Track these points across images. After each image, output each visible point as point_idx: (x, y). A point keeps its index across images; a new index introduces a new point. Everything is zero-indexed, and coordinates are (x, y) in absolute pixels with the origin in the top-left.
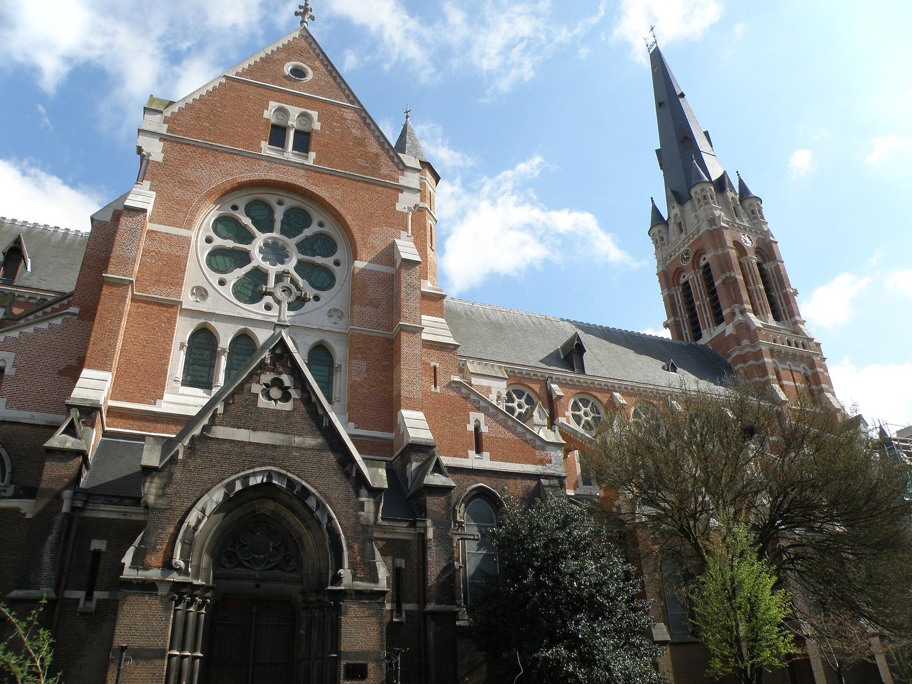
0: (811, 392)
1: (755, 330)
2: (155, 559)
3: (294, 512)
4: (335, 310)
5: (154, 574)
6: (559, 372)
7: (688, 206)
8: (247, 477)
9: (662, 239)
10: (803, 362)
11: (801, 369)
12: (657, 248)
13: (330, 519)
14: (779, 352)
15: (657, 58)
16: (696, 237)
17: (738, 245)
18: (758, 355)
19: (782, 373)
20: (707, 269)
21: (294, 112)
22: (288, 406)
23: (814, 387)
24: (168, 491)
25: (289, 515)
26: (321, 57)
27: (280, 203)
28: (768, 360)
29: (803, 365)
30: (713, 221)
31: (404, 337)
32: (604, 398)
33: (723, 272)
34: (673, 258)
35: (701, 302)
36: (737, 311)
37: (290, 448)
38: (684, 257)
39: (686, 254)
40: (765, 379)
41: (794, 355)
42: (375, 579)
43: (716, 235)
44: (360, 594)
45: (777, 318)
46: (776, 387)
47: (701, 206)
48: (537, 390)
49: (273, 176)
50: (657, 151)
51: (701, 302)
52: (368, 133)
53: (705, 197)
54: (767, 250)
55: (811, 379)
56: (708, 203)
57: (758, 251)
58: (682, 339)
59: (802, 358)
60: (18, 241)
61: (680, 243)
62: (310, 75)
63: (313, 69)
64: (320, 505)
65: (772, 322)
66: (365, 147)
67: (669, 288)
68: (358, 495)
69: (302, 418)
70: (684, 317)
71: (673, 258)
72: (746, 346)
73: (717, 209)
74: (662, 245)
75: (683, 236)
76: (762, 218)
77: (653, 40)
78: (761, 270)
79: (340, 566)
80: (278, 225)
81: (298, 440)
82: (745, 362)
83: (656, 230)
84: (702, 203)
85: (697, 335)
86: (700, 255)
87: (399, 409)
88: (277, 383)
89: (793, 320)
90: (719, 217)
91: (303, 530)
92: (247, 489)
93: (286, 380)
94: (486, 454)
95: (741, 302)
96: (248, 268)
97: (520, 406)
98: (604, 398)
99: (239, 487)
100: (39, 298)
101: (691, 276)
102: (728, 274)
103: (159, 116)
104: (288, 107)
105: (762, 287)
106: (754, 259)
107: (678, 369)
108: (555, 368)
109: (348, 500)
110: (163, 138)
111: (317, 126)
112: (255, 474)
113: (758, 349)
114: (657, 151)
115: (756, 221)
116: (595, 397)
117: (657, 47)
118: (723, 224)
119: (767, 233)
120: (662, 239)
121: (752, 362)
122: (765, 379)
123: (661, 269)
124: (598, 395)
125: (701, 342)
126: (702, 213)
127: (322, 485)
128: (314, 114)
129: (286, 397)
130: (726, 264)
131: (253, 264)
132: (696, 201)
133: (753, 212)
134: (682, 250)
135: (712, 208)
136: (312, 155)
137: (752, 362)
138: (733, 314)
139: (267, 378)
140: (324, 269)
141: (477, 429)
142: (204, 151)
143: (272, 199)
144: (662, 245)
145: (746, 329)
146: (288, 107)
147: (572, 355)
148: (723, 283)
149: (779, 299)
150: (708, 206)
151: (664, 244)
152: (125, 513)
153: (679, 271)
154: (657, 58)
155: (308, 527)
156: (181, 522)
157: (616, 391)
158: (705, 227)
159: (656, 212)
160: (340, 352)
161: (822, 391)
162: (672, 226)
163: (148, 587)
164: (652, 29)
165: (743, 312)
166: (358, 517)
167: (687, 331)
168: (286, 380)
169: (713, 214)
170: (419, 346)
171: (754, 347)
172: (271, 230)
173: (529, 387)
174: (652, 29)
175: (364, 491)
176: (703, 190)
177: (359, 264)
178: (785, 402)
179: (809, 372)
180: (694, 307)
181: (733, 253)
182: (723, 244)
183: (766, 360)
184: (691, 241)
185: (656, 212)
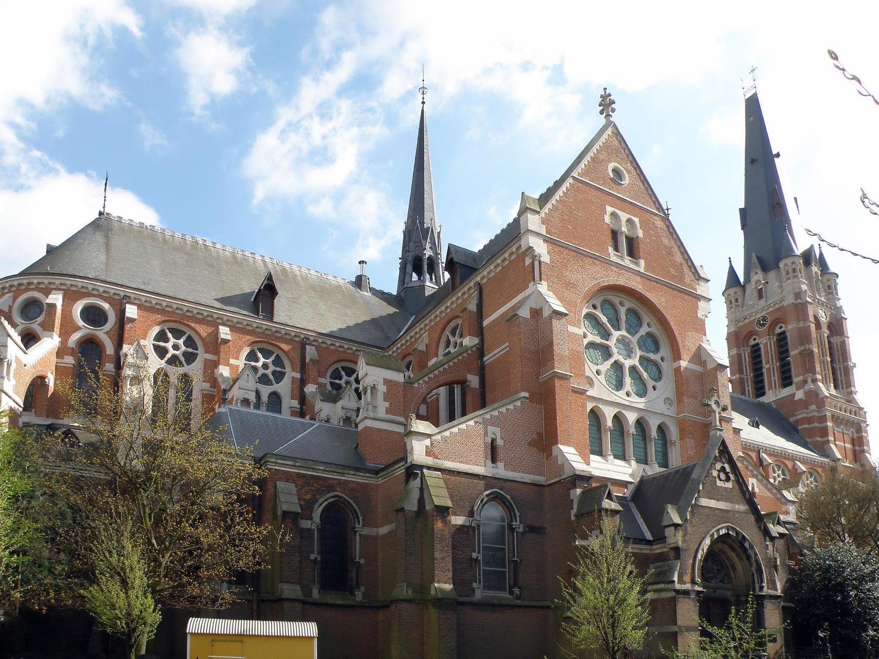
0: (854, 451)
1: (823, 398)
2: (687, 578)
3: (734, 550)
4: (668, 398)
5: (688, 586)
6: (243, 316)
7: (772, 275)
8: (718, 530)
9: (737, 300)
10: (852, 426)
11: (850, 433)
12: (729, 308)
13: (756, 554)
14: (838, 418)
15: (753, 107)
16: (777, 306)
17: (816, 318)
18: (823, 419)
19: (837, 434)
20: (782, 339)
21: (624, 216)
22: (729, 485)
23: (857, 448)
24: (687, 538)
25: (732, 555)
26: (631, 158)
27: (649, 325)
28: (830, 424)
29: (851, 430)
30: (798, 295)
31: (558, 383)
32: (790, 464)
33: (802, 344)
34: (747, 321)
35: (770, 366)
36: (809, 380)
37: (734, 512)
38: (762, 322)
39: (763, 320)
40: (825, 439)
41: (848, 421)
42: (776, 590)
43: (800, 309)
44: (771, 597)
45: (836, 387)
46: (833, 446)
47: (789, 279)
48: (754, 457)
49: (622, 281)
50: (741, 210)
51: (770, 366)
52: (673, 242)
53: (794, 270)
54: (837, 326)
55: (856, 442)
56: (796, 277)
57: (830, 326)
58: (743, 393)
59: (848, 423)
60: (270, 278)
61: (757, 309)
62: (611, 166)
63: (629, 172)
64: (751, 547)
65: (833, 391)
66: (673, 256)
67: (738, 347)
68: (765, 541)
69: (737, 493)
70: (749, 375)
71: (747, 321)
72: (813, 411)
73: (804, 283)
74: (736, 306)
75: (762, 301)
76: (837, 294)
77: (753, 83)
78: (829, 342)
79: (762, 582)
80: (638, 335)
81: (737, 506)
82: (809, 424)
83: (732, 291)
84: (791, 275)
85: (760, 391)
86: (777, 324)
87: (556, 443)
88: (723, 469)
89: (849, 390)
90: (806, 291)
91: (736, 560)
92: (720, 537)
93: (728, 469)
94: (500, 465)
95: (814, 372)
96: (611, 361)
97: (176, 347)
98: (204, 331)
99: (716, 536)
100: (302, 336)
101: (767, 343)
102: (807, 346)
103: (537, 216)
104: (619, 212)
105: (829, 359)
106: (826, 332)
107: (761, 426)
108: (246, 313)
109: (761, 543)
110: (546, 240)
111: (640, 233)
112: (721, 528)
113: (823, 414)
114: (741, 210)
115: (831, 296)
116: (194, 329)
117: (755, 95)
118: (808, 299)
119: (839, 310)
120: (737, 300)
121: (816, 424)
122: (825, 439)
123: (733, 329)
124: (197, 327)
125: (764, 399)
126: (789, 285)
127: (751, 534)
128: (636, 220)
129: (728, 479)
130: (804, 337)
131: (638, 364)
132: (784, 273)
133: (829, 287)
134: (759, 315)
135: (800, 282)
136: (642, 262)
137: (816, 424)
138: (805, 382)
139: (718, 466)
140: (655, 363)
141: (493, 441)
142: (575, 254)
143: (616, 300)
144: (736, 306)
145: (814, 397)
146: (619, 212)
147: (266, 295)
148: (800, 353)
149: (841, 372)
150: (796, 280)
151: (738, 306)
152: (641, 549)
153: (751, 334)
154: (753, 107)
155: (741, 559)
156: (695, 557)
157: (224, 325)
158: (790, 300)
159: (732, 272)
160: (674, 432)
161: (863, 451)
162: (751, 289)
163: (686, 593)
164: (753, 71)
165: (814, 381)
166: (766, 553)
167: (750, 388)
168: (726, 466)
169: (800, 288)
170: (732, 432)
171: (818, 412)
172: (633, 335)
173: (190, 327)
174: (753, 71)
175: (767, 538)
176: (793, 263)
177: (684, 364)
178: (839, 459)
179: (856, 436)
180: (761, 368)
181: (813, 326)
182: (806, 318)
183: (828, 424)
184: (771, 309)
185: (732, 272)
